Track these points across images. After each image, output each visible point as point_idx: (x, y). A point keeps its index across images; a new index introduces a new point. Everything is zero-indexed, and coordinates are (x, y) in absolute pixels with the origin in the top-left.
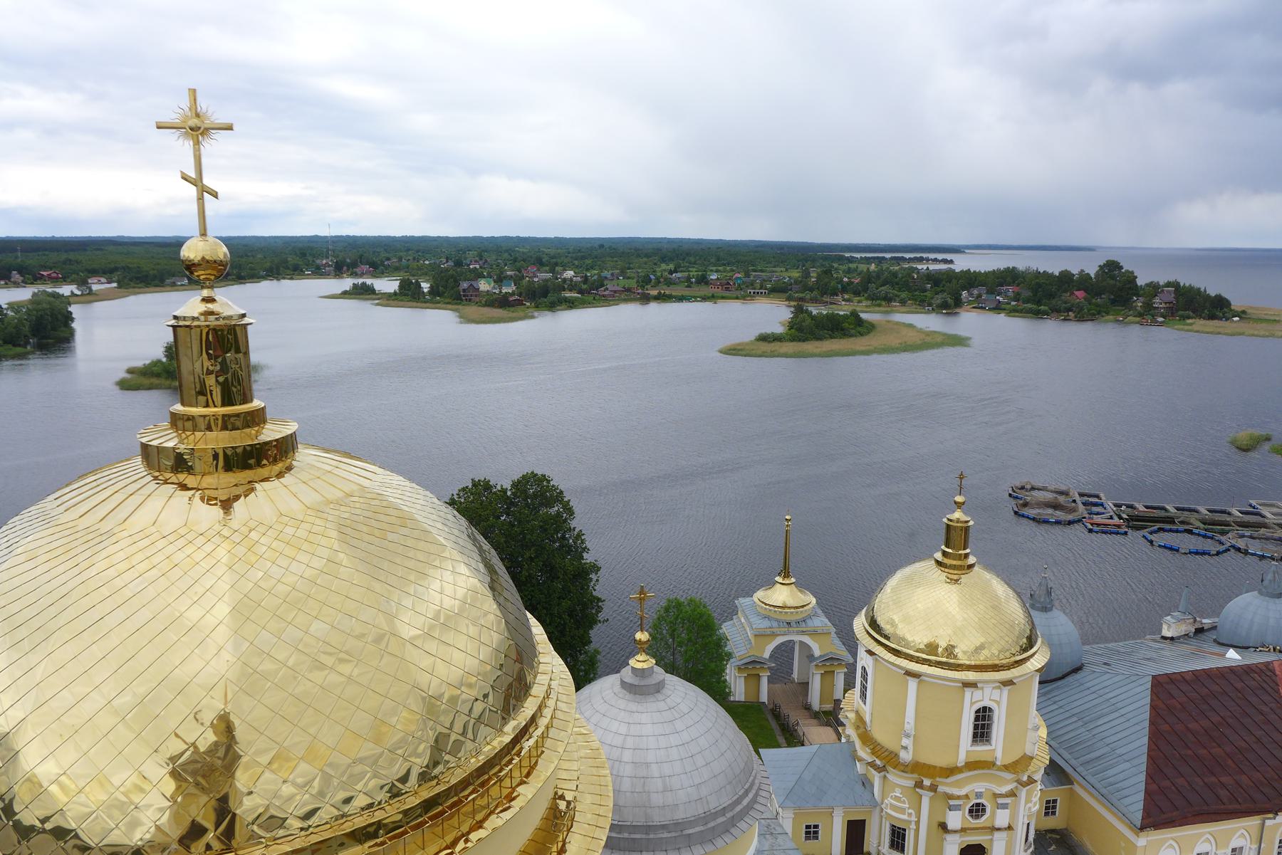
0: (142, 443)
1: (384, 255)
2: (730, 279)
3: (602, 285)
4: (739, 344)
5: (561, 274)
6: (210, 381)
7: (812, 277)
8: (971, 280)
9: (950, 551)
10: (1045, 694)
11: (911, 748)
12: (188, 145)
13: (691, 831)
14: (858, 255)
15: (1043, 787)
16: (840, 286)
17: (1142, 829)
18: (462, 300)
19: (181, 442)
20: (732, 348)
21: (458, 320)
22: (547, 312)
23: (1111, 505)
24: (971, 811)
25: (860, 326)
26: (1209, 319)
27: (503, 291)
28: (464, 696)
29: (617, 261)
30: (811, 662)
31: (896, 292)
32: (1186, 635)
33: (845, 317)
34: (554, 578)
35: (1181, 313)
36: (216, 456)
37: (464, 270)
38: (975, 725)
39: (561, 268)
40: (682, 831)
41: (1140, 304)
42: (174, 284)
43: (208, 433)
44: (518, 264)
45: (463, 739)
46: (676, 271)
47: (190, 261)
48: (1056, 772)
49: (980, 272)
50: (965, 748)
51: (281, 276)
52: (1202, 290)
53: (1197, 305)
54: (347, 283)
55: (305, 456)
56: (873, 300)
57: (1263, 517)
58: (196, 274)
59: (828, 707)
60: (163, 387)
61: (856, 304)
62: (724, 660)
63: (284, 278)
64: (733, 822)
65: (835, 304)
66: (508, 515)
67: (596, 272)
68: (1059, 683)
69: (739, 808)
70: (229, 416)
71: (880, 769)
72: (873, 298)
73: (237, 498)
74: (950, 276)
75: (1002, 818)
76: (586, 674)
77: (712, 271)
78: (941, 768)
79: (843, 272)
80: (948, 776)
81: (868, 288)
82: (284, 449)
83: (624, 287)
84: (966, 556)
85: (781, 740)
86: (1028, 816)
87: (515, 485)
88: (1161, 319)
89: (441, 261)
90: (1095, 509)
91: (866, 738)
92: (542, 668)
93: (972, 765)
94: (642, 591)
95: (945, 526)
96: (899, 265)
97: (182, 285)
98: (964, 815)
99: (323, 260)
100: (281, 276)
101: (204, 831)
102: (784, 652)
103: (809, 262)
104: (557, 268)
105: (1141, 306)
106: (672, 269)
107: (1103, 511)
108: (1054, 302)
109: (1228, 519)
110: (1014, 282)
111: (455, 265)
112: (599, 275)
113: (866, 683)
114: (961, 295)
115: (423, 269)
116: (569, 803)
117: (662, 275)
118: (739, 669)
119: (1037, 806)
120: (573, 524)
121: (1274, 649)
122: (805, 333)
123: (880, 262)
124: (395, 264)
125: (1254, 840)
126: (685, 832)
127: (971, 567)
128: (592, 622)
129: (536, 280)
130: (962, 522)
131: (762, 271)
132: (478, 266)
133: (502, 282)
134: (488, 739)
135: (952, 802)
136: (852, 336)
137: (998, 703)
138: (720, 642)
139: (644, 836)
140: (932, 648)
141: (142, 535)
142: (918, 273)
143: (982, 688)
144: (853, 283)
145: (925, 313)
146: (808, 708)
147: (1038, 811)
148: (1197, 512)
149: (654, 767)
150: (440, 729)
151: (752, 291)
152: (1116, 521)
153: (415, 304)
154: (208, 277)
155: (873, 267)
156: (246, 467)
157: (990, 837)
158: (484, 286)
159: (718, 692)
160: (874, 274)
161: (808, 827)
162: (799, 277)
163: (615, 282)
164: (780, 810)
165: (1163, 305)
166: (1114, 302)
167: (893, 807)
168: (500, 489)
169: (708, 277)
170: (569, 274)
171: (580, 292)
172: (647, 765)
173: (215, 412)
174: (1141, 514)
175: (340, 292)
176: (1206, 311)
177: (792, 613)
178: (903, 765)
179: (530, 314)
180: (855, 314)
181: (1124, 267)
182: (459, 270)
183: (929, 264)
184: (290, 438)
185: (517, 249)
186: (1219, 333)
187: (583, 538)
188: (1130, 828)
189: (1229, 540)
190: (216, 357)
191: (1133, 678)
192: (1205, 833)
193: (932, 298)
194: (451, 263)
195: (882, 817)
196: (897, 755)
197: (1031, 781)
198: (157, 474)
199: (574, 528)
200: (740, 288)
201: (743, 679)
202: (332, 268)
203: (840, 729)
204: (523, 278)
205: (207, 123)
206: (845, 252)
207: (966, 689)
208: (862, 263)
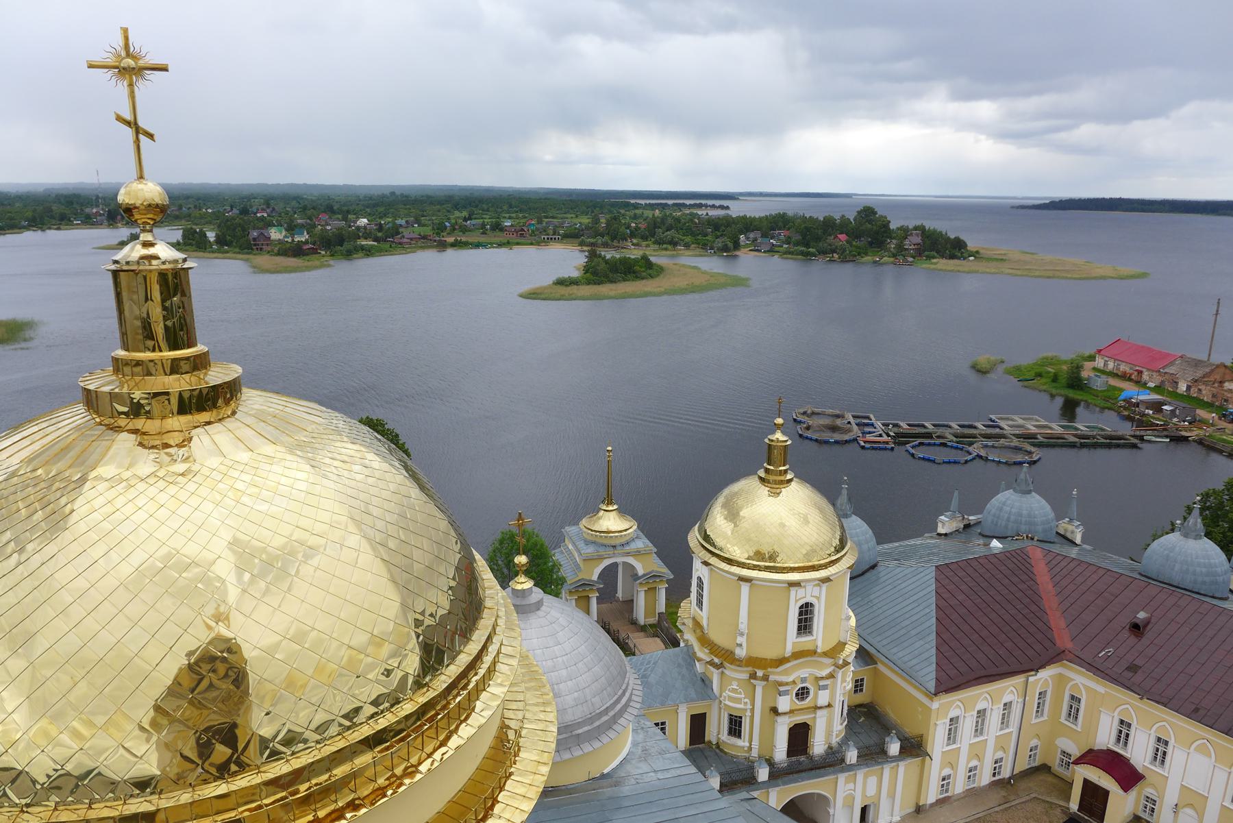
2: (524, 226)
3: (398, 233)
8: (747, 225)
9: (772, 468)
11: (744, 645)
12: (122, 88)
13: (580, 731)
14: (643, 202)
17: (935, 695)
18: (252, 249)
20: (532, 292)
22: (343, 260)
23: (880, 424)
24: (797, 695)
25: (650, 269)
26: (950, 259)
27: (296, 240)
30: (635, 580)
31: (681, 236)
32: (956, 531)
33: (636, 260)
35: (926, 253)
37: (251, 219)
38: (799, 619)
39: (354, 216)
40: (571, 732)
41: (893, 246)
44: (309, 212)
46: (470, 219)
48: (864, 655)
49: (755, 218)
51: (45, 227)
52: (944, 233)
53: (939, 247)
56: (659, 244)
57: (1002, 429)
61: (645, 248)
63: (50, 228)
65: (625, 248)
69: (619, 707)
72: (659, 242)
75: (823, 698)
77: (505, 217)
78: (771, 660)
79: (630, 217)
80: (778, 667)
81: (654, 234)
83: (420, 235)
84: (786, 472)
88: (911, 259)
89: (225, 209)
90: (867, 429)
91: (705, 641)
93: (798, 655)
95: (767, 447)
96: (681, 211)
98: (792, 698)
99: (93, 209)
100: (46, 227)
102: (609, 574)
105: (894, 248)
107: (874, 430)
108: (821, 244)
109: (975, 432)
110: (784, 227)
113: (702, 591)
114: (739, 239)
117: (456, 222)
118: (570, 592)
121: (1027, 537)
122: (600, 277)
123: (663, 208)
125: (1020, 694)
126: (574, 733)
129: (328, 228)
131: (553, 217)
132: (265, 215)
135: (782, 689)
136: (643, 279)
137: (818, 598)
142: (699, 219)
143: (805, 587)
144: (640, 228)
146: (634, 623)
147: (850, 690)
148: (950, 427)
151: (546, 237)
152: (885, 438)
153: (201, 254)
157: (813, 715)
162: (589, 223)
163: (410, 229)
165: (912, 247)
166: (871, 244)
167: (731, 699)
169: (502, 223)
170: (363, 221)
171: (376, 239)
174: (905, 431)
175: (117, 243)
176: (947, 251)
177: (616, 537)
180: (645, 258)
181: (878, 213)
182: (245, 218)
183: (708, 210)
189: (976, 449)
192: (983, 693)
193: (714, 242)
194: (235, 211)
195: (720, 708)
196: (732, 653)
197: (846, 664)
202: (104, 218)
204: (314, 226)
205: (141, 63)
207: (791, 588)
208: (647, 210)
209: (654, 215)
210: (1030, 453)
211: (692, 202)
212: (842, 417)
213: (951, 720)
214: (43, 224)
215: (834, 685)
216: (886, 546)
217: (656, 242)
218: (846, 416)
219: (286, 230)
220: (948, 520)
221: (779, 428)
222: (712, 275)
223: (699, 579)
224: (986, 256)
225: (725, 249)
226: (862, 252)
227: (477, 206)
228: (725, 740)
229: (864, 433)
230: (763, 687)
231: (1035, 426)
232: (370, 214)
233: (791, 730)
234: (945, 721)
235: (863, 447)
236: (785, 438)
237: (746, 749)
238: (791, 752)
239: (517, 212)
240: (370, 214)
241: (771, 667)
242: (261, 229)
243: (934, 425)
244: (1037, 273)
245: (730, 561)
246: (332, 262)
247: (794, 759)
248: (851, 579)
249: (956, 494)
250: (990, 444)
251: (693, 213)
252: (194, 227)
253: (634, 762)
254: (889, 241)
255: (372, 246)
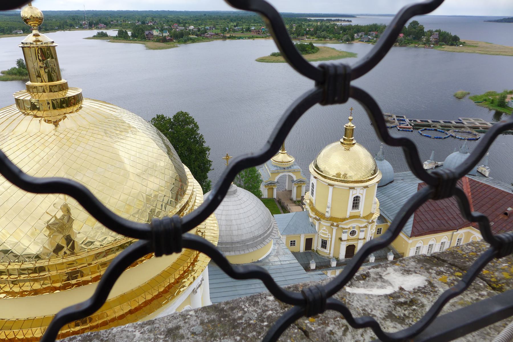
0: (15, 98)
1: (110, 19)
3: (206, 32)
4: (264, 57)
5: (188, 27)
6: (42, 72)
7: (294, 28)
8: (358, 29)
10: (379, 191)
11: (329, 212)
13: (248, 243)
14: (313, 19)
15: (377, 224)
16: (305, 32)
17: (411, 237)
18: (146, 39)
19: (33, 97)
21: (145, 48)
23: (408, 120)
24: (351, 233)
25: (313, 49)
28: (160, 195)
29: (212, 22)
30: (293, 182)
32: (432, 168)
34: (192, 153)
35: (440, 43)
36: (48, 103)
39: (188, 25)
41: (425, 39)
42: (16, 33)
43: (44, 93)
44: (170, 23)
45: (160, 210)
46: (237, 26)
47: (26, 17)
50: (350, 211)
51: (65, 29)
52: (449, 34)
54: (95, 32)
55: (86, 103)
58: (29, 23)
59: (299, 199)
60: (16, 79)
62: (259, 183)
63: (66, 30)
64: (264, 240)
66: (172, 129)
67: (203, 26)
68: (386, 186)
69: (266, 235)
70: (52, 86)
71: (318, 220)
72: (318, 37)
73: (60, 120)
74: (350, 28)
76: (206, 190)
77: (252, 26)
78: (340, 219)
82: (75, 101)
84: (352, 140)
85: (281, 211)
86: (371, 234)
87: (175, 117)
88: (432, 46)
90: (402, 122)
91: (313, 209)
92: (189, 184)
93: (351, 217)
94: (227, 155)
97: (20, 34)
98: (348, 235)
101: (63, 247)
103: (293, 22)
104: (186, 25)
106: (236, 25)
107: (405, 123)
110: (375, 30)
111: (142, 24)
112: (205, 28)
115: (128, 26)
116: (202, 233)
118: (265, 186)
119: (374, 231)
120: (198, 132)
123: (322, 22)
124: (115, 23)
126: (246, 244)
127: (354, 144)
128: (208, 170)
129: (177, 30)
130: (351, 127)
132: (152, 24)
133: (163, 31)
134: (170, 210)
135: (344, 231)
136: (310, 53)
137: (362, 194)
138: (258, 176)
139: (231, 246)
140: (338, 175)
141: (21, 136)
142: (337, 26)
143: (356, 189)
144: (311, 30)
145: (340, 43)
146: (291, 200)
148: (439, 122)
149: (234, 221)
150: (152, 207)
152: (409, 126)
154: (35, 24)
155: (319, 24)
156: (62, 107)
158: (155, 33)
159: (258, 195)
160: (319, 27)
161: (291, 241)
163: (211, 31)
164: (281, 236)
166: (414, 38)
167: (323, 233)
168: (168, 118)
170: (192, 27)
171: (197, 35)
172: (231, 220)
173: (46, 84)
175: (92, 36)
178: (326, 218)
179: (176, 45)
180: (311, 44)
182: (144, 26)
184: (79, 95)
185: (169, 16)
186: (454, 51)
187: (203, 137)
188: (407, 237)
189: (450, 133)
190: (43, 60)
191: (412, 184)
193: (343, 37)
196: (324, 215)
197: (373, 222)
198: (24, 111)
199: (199, 133)
200: (264, 33)
201: (267, 190)
202: (87, 25)
203: (304, 206)
204: (172, 29)
206: (307, 17)
209: (317, 24)
210: (475, 135)
211: (335, 19)
212: (391, 116)
213: (417, 248)
214: (64, 28)
215: (367, 231)
216: (396, 173)
217: (317, 37)
218: (393, 116)
219: (160, 31)
220: (428, 163)
221: (350, 121)
222: (340, 52)
223: (313, 184)
224: (468, 44)
225: (347, 40)
226: (409, 42)
227: (240, 21)
228: (320, 249)
229: (400, 124)
230: (336, 229)
231: (479, 123)
232: (195, 24)
233: (347, 247)
234: (427, 245)
235: (399, 130)
236: (353, 125)
237: (328, 253)
238: (346, 256)
239: (257, 23)
240: (195, 24)
241: (340, 222)
242: (150, 30)
243: (433, 121)
244: (492, 53)
245: (325, 177)
246: (178, 45)
247: (348, 259)
248: (378, 187)
249: (433, 152)
250: (457, 130)
251: (335, 24)
252: (123, 29)
253: (272, 257)
254: (423, 37)
255: (195, 38)
